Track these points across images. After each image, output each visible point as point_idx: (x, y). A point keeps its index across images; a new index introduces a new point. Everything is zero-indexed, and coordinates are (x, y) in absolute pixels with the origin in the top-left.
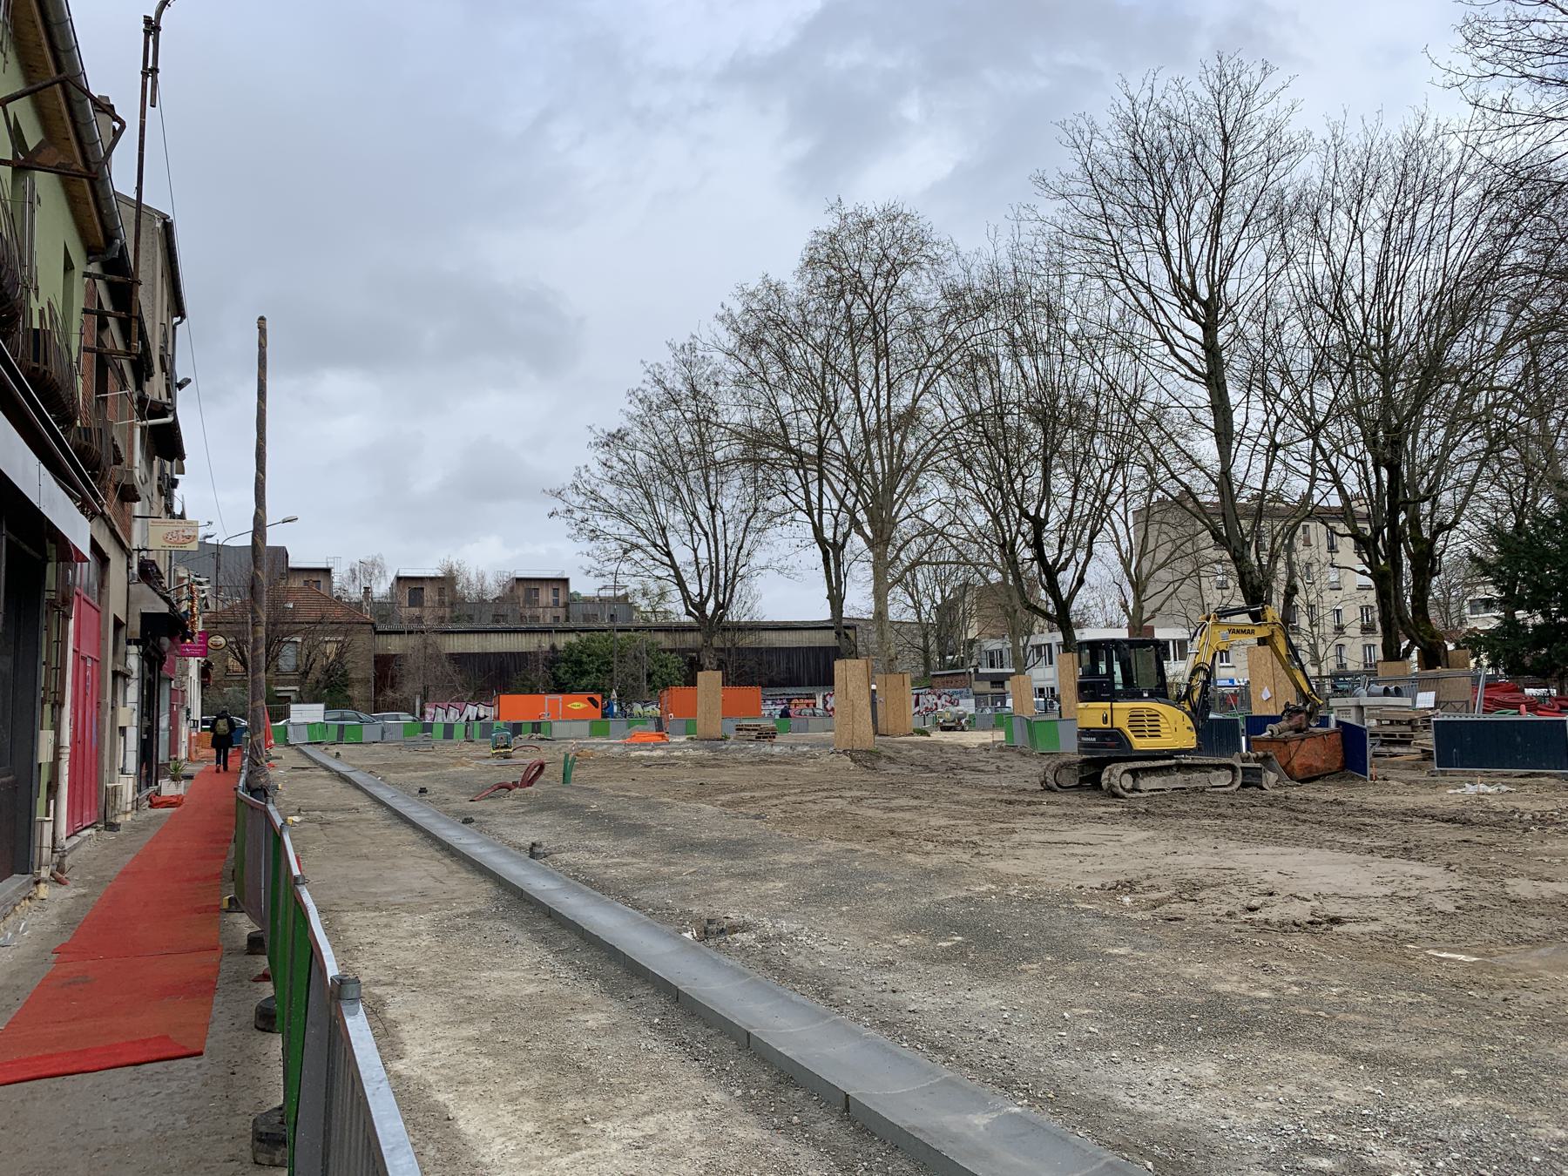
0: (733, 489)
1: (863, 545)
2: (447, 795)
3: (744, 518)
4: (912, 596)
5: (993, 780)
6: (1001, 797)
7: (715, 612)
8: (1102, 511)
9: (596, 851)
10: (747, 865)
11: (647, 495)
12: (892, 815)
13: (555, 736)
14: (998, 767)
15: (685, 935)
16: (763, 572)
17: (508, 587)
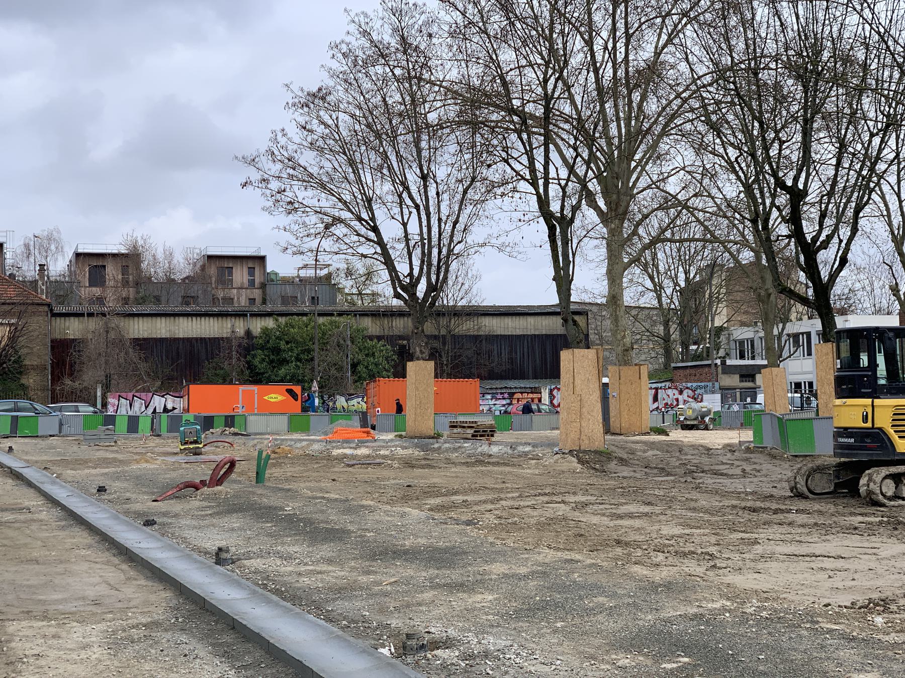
0: (446, 156)
1: (597, 219)
2: (128, 495)
3: (461, 189)
4: (652, 278)
5: (737, 485)
6: (743, 504)
7: (427, 294)
8: (870, 180)
9: (288, 558)
10: (455, 575)
11: (352, 162)
12: (620, 522)
13: (251, 430)
14: (744, 471)
15: (381, 650)
16: (482, 250)
17: (198, 266)
